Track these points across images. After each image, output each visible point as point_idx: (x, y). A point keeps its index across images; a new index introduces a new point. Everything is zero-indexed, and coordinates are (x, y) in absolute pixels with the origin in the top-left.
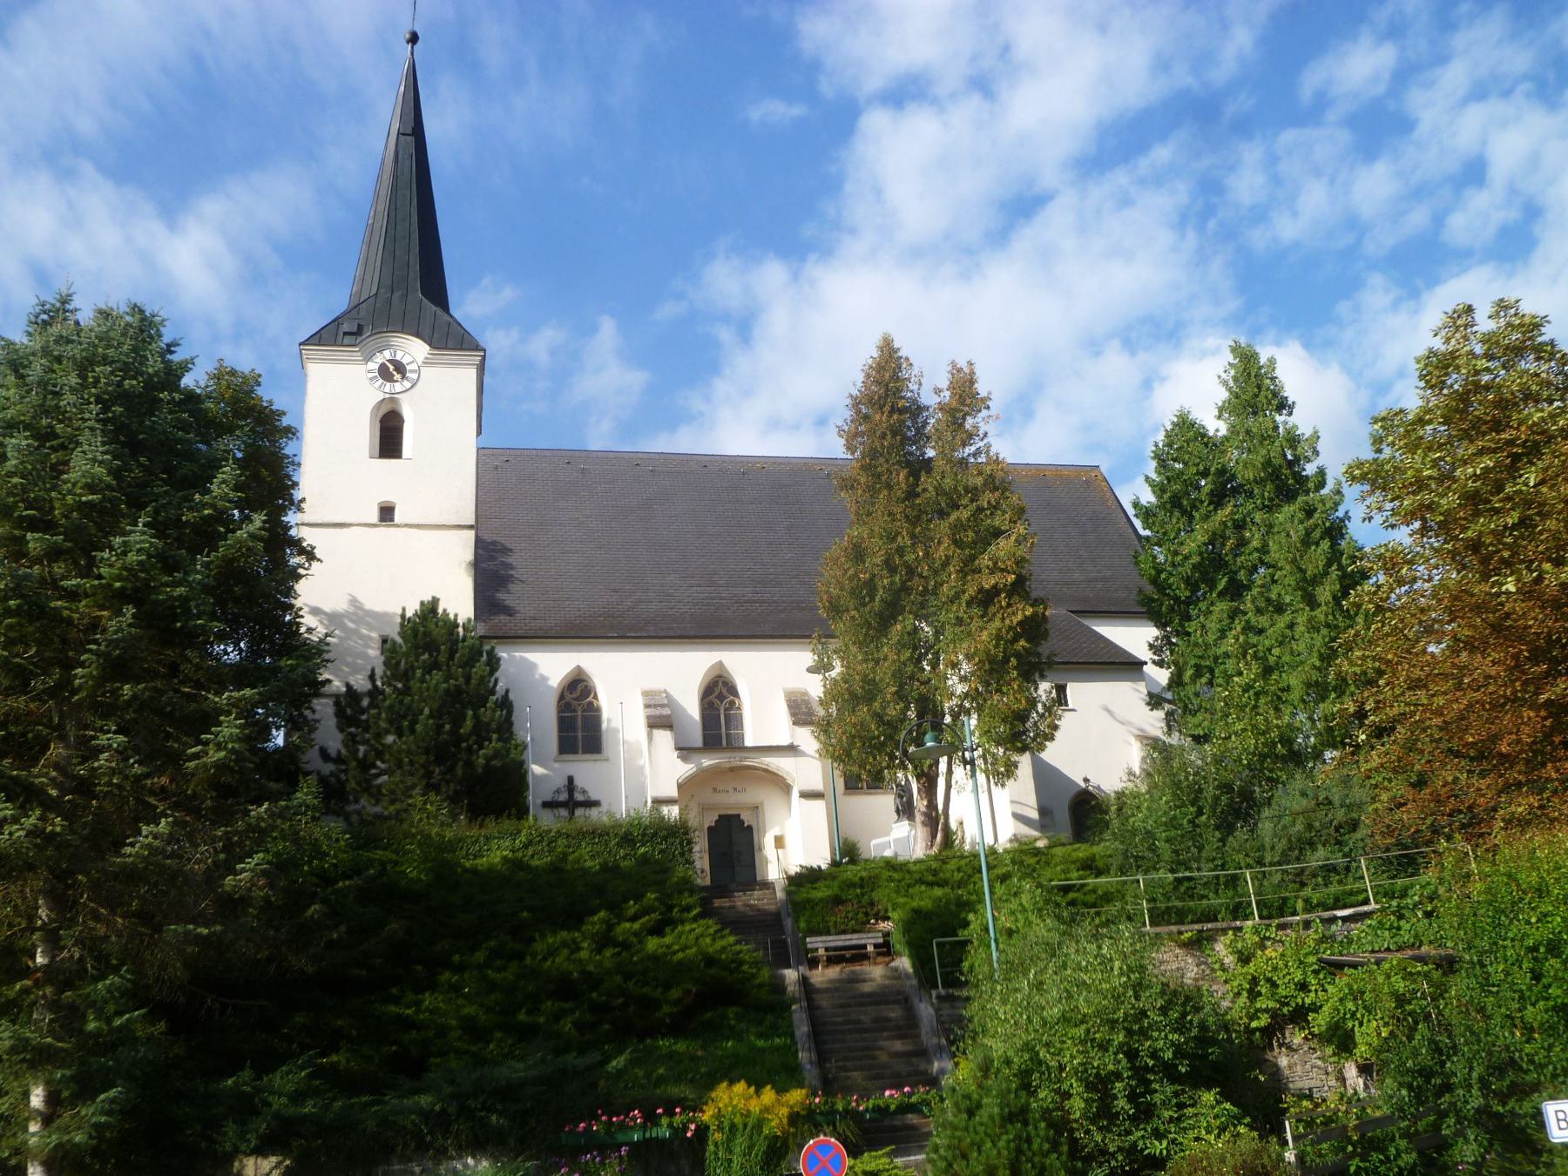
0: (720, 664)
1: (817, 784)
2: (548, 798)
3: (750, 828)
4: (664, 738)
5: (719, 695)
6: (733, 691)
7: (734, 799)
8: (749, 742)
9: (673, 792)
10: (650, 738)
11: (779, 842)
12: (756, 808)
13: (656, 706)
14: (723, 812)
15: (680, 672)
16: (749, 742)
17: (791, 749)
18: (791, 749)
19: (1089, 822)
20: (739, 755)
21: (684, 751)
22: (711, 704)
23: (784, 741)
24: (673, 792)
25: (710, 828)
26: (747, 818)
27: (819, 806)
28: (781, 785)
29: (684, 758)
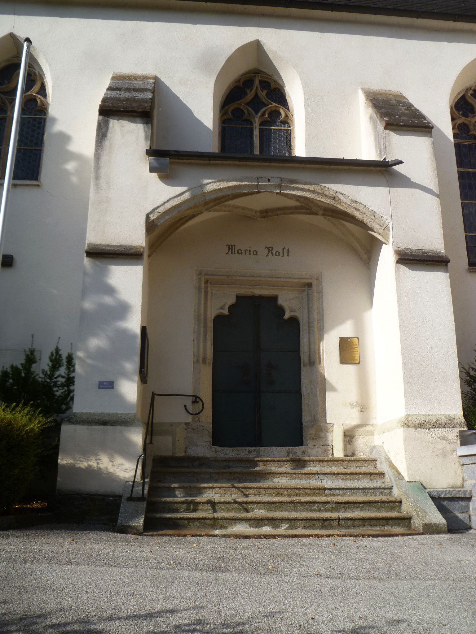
0: (257, 45)
1: (433, 239)
2: (417, 422)
3: (294, 322)
4: (131, 137)
5: (253, 99)
6: (278, 95)
7: (266, 267)
8: (300, 150)
9: (137, 237)
10: (102, 133)
11: (348, 351)
12: (308, 287)
13: (119, 89)
14: (244, 291)
15: (189, 60)
16: (300, 150)
17: (381, 171)
18: (381, 171)
19: (59, 392)
20: (275, 174)
21: (166, 158)
22: (238, 114)
23: (367, 151)
24: (137, 237)
25: (218, 319)
26: (288, 302)
27: (437, 282)
28: (360, 243)
29: (167, 176)
